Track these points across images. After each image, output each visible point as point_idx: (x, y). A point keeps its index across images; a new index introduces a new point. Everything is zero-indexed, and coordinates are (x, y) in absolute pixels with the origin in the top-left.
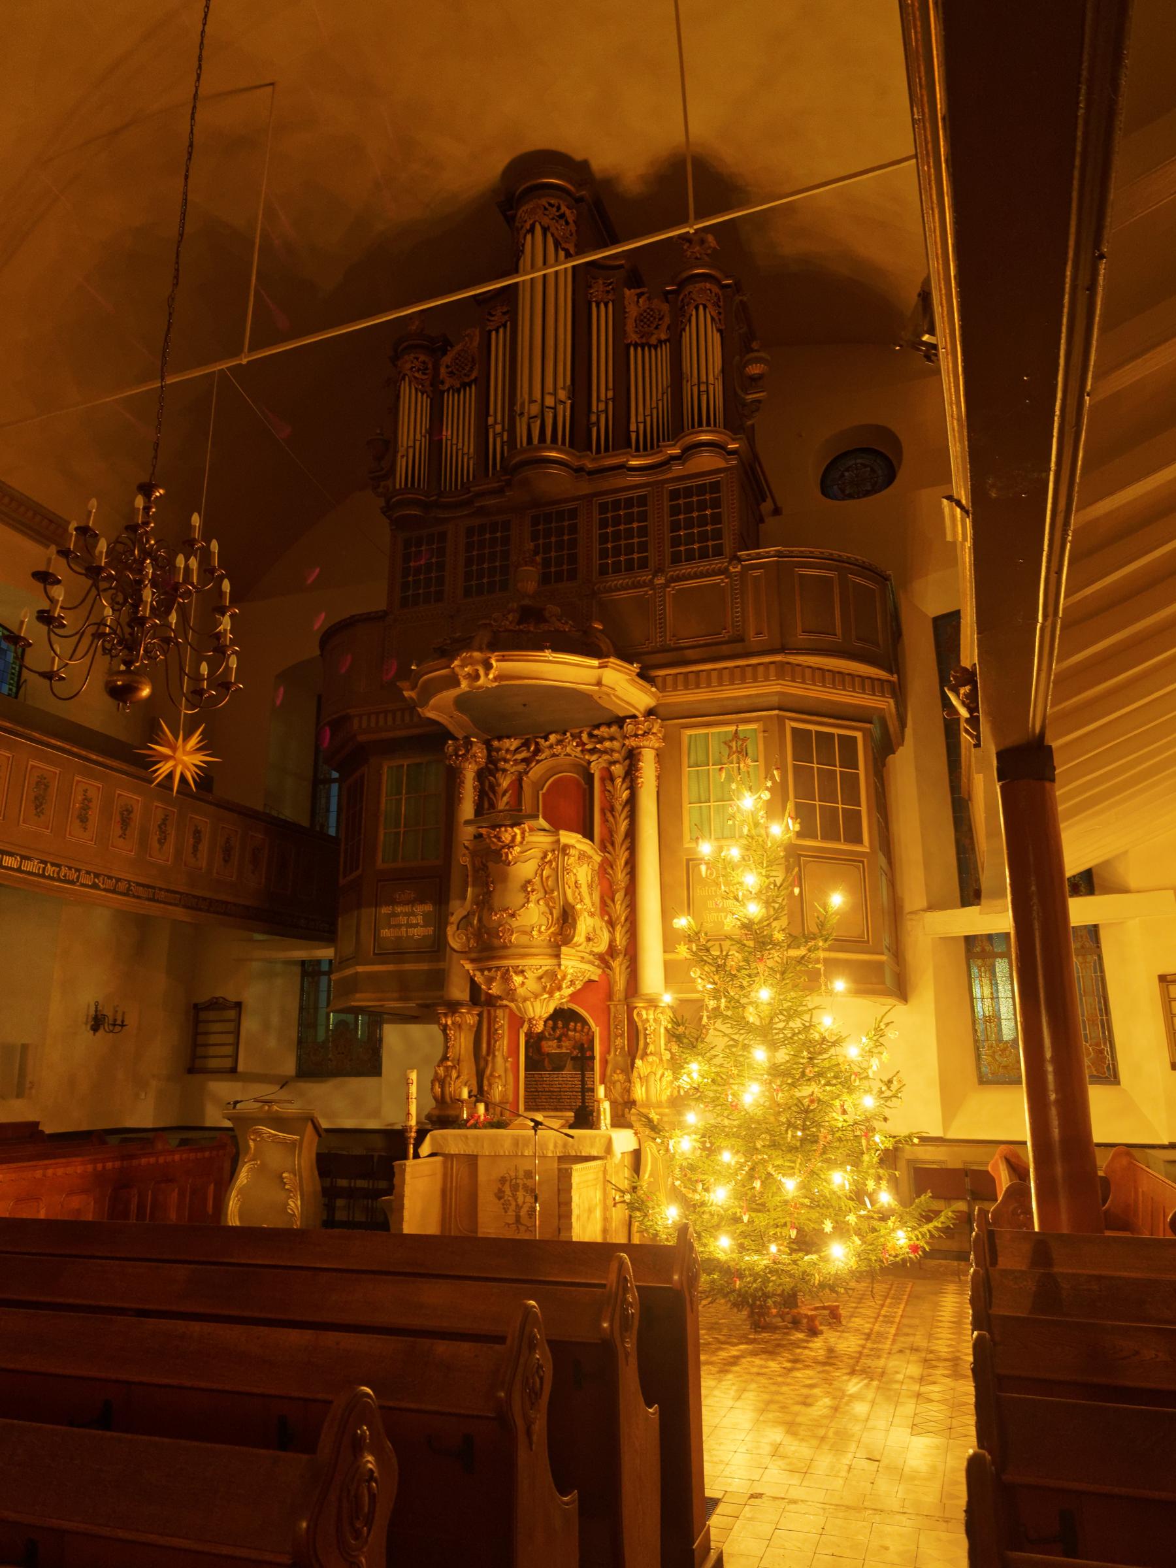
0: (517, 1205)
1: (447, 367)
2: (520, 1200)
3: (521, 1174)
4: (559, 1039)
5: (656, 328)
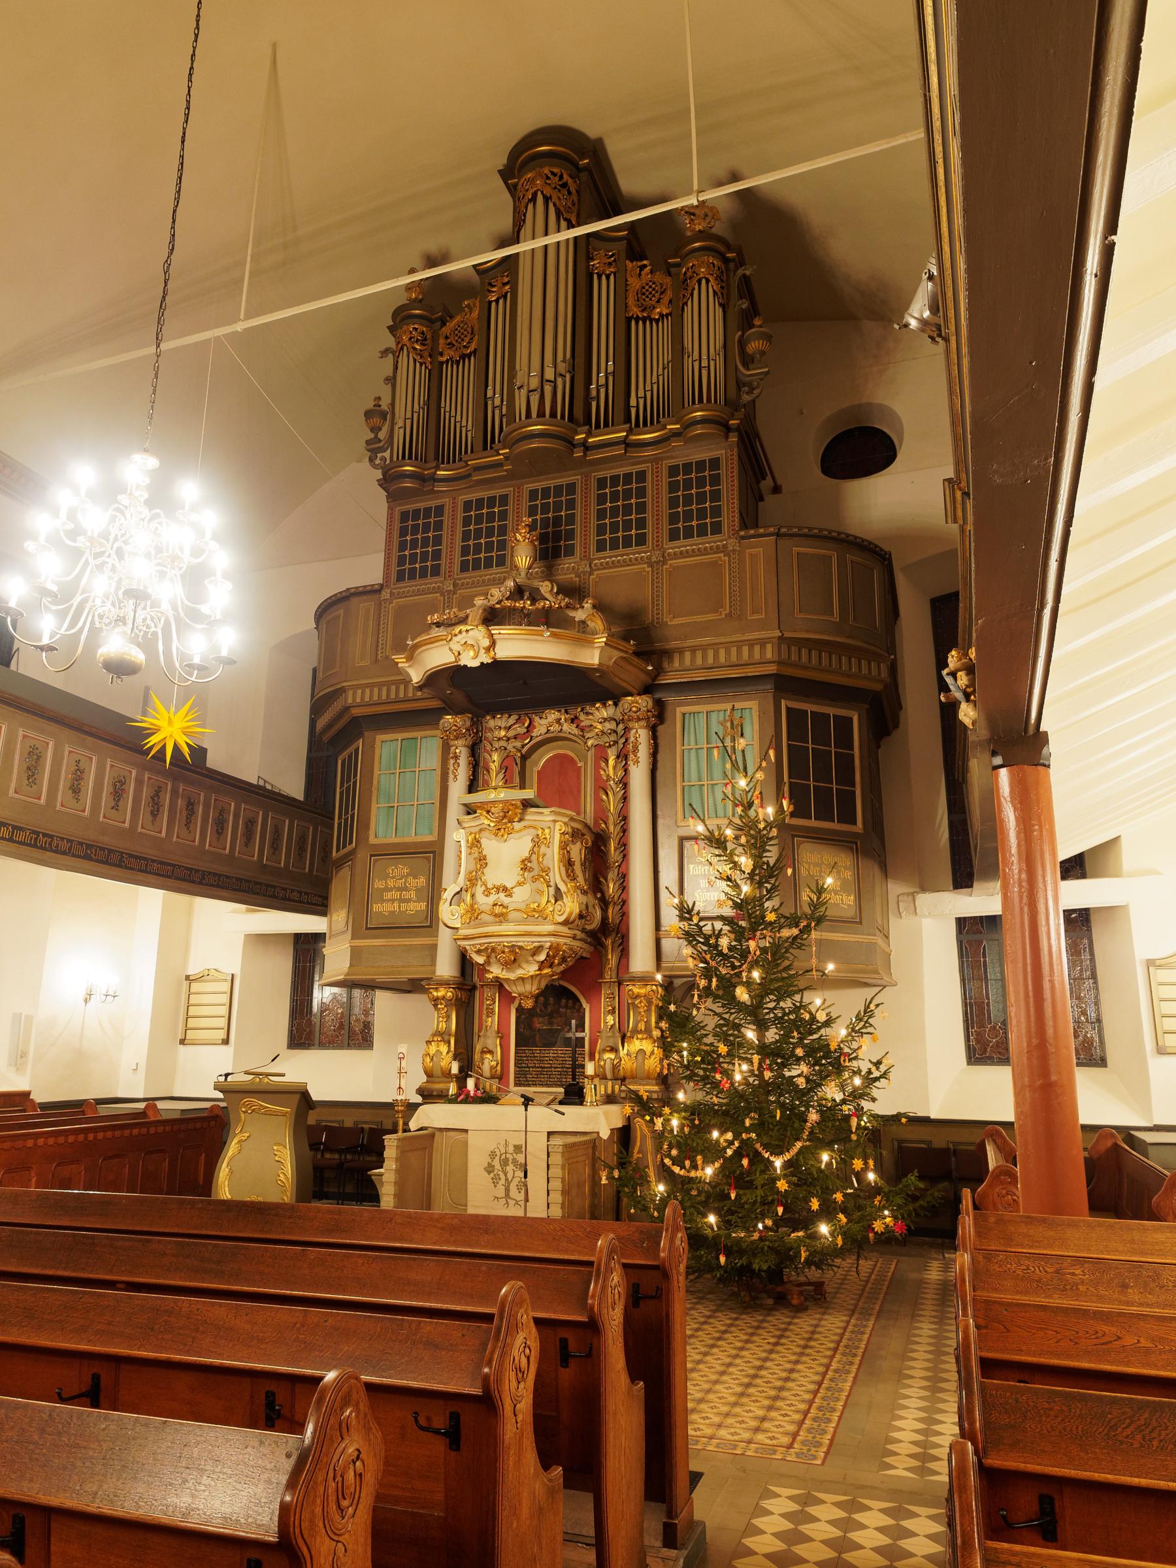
0: (507, 1179)
1: (447, 338)
2: (510, 1176)
3: (511, 1149)
4: (551, 1016)
5: (658, 301)
